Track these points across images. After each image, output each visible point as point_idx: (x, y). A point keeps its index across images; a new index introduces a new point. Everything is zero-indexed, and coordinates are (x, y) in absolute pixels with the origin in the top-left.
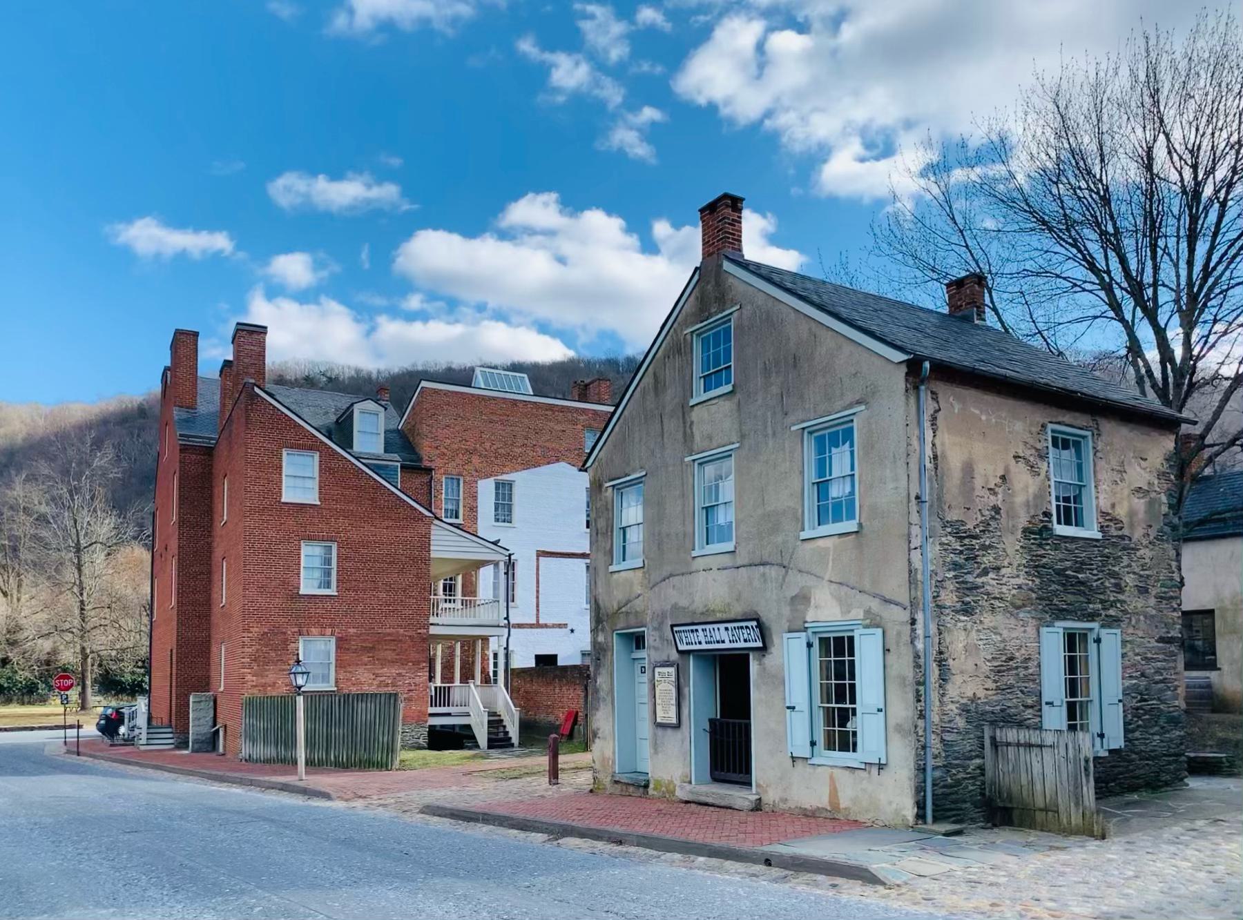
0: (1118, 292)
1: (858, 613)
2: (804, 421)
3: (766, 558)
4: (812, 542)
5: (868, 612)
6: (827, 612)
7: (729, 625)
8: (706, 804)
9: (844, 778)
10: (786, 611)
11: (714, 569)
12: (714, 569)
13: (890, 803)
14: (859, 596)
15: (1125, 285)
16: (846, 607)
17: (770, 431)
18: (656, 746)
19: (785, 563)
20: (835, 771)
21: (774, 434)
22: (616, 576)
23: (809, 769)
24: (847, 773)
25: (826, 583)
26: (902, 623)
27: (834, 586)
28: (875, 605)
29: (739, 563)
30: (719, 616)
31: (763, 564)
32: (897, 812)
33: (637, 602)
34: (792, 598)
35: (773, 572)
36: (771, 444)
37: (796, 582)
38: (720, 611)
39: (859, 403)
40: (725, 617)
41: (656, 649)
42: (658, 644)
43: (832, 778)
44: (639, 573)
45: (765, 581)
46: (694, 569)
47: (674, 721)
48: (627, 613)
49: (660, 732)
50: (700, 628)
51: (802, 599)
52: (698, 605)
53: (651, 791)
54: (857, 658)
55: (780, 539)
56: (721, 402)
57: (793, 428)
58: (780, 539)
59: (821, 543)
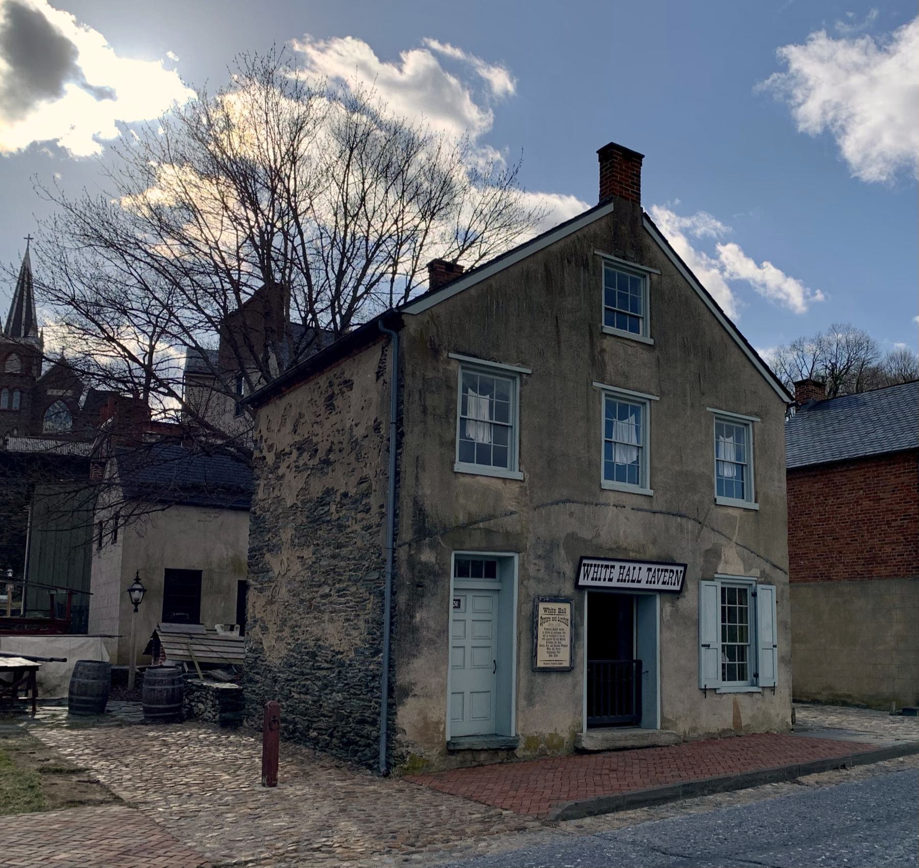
0: (53, 443)
1: (756, 572)
2: (717, 408)
3: (683, 512)
4: (726, 508)
5: (763, 572)
6: (733, 567)
7: (653, 567)
8: (625, 749)
9: (744, 701)
10: (700, 561)
11: (628, 508)
12: (628, 508)
13: (778, 715)
14: (757, 559)
15: (59, 443)
16: (748, 567)
17: (689, 402)
18: (530, 699)
19: (701, 520)
20: (739, 697)
21: (692, 406)
22: (463, 480)
23: (717, 698)
24: (747, 697)
25: (732, 544)
26: (785, 584)
27: (739, 548)
28: (768, 568)
29: (656, 508)
30: (632, 555)
31: (680, 516)
32: (783, 720)
33: (508, 519)
34: (707, 551)
35: (690, 525)
36: (688, 413)
37: (710, 539)
38: (633, 551)
39: (757, 415)
40: (639, 557)
41: (539, 580)
42: (542, 574)
43: (736, 705)
44: (515, 487)
45: (682, 532)
46: (602, 500)
47: (566, 664)
48: (488, 531)
49: (539, 679)
50: (618, 565)
51: (714, 554)
52: (605, 539)
53: (519, 753)
54: (720, 605)
55: (696, 498)
56: (639, 349)
57: (708, 409)
58: (696, 498)
59: (730, 511)
